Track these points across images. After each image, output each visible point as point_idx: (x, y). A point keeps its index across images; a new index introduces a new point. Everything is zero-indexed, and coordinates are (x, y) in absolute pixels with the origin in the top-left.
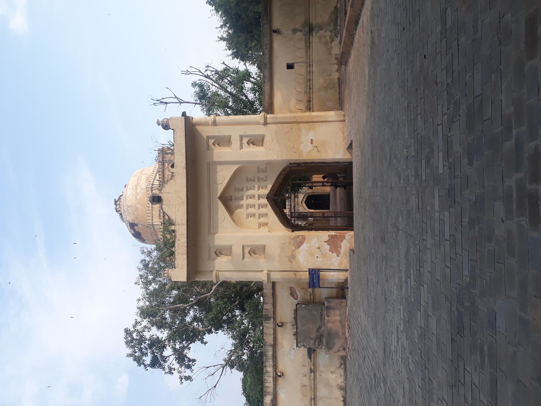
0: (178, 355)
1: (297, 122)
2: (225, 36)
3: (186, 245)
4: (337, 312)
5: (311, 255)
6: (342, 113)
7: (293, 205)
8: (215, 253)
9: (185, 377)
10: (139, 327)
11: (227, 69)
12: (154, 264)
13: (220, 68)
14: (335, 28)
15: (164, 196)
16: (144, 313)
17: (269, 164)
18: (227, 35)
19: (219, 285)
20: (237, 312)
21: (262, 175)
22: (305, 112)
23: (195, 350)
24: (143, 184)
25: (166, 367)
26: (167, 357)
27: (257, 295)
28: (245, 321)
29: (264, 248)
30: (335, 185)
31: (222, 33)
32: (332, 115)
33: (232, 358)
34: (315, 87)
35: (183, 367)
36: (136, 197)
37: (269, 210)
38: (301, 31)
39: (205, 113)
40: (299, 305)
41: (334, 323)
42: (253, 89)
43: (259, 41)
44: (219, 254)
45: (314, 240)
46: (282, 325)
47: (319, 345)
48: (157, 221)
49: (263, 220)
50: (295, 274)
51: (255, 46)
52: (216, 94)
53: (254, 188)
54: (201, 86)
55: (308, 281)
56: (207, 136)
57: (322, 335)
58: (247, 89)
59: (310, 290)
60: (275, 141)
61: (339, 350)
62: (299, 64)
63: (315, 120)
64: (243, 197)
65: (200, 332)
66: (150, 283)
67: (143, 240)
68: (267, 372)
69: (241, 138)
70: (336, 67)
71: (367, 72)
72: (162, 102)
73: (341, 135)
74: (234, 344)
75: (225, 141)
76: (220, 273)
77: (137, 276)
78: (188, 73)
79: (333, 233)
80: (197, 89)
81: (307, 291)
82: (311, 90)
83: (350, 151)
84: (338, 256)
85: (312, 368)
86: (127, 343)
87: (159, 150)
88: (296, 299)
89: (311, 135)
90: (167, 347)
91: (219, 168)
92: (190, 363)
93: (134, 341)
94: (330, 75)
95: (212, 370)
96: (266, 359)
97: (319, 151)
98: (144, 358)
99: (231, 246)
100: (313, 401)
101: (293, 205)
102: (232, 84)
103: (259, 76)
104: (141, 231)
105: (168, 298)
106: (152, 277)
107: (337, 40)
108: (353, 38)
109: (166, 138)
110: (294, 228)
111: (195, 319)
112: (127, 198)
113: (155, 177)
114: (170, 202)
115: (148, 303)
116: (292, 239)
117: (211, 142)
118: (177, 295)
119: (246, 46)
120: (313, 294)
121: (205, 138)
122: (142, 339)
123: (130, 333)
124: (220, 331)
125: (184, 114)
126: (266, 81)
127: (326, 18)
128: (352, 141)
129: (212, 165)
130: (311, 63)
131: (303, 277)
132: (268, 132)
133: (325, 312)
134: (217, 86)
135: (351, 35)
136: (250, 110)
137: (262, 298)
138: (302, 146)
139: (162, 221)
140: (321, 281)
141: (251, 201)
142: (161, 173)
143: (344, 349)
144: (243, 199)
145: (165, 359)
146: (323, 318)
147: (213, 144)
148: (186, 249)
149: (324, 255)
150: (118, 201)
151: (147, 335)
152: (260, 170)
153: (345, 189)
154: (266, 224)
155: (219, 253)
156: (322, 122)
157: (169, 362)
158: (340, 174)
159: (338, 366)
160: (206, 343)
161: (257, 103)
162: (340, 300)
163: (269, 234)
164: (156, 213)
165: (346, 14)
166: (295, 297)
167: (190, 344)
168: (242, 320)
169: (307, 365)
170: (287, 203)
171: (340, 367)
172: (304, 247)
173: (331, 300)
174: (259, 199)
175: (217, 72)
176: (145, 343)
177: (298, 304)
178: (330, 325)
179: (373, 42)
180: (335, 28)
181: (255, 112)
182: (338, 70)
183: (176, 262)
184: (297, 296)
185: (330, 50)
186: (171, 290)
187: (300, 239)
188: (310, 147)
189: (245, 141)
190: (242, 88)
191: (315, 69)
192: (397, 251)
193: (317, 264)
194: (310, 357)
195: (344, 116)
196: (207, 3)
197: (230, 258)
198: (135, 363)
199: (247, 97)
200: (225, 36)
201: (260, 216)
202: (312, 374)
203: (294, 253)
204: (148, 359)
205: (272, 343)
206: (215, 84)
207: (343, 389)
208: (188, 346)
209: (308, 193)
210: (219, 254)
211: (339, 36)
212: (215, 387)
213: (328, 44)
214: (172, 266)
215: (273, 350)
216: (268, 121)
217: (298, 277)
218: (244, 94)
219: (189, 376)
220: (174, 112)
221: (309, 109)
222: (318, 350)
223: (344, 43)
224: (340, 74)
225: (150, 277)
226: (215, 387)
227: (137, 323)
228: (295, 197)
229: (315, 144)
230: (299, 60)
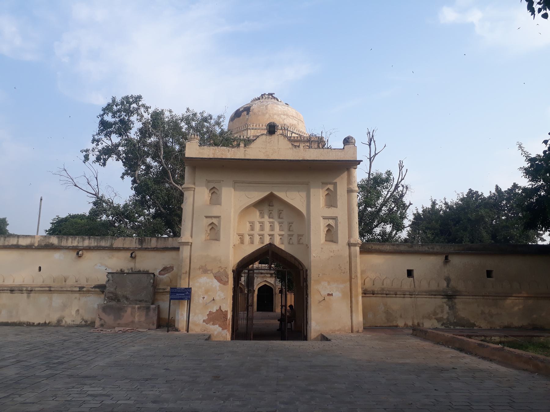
0: (112, 149)
2: (437, 207)
3: (224, 157)
4: (143, 319)
5: (207, 292)
6: (361, 329)
7: (263, 271)
8: (214, 187)
9: (88, 155)
10: (142, 110)
11: (405, 207)
12: (207, 127)
13: (406, 200)
14: (451, 324)
15: (275, 137)
16: (157, 116)
18: (438, 209)
19: (181, 192)
20: (152, 211)
21: (295, 239)
22: (362, 288)
23: (116, 166)
24: (288, 121)
26: (110, 137)
27: (170, 231)
28: (142, 218)
29: (217, 239)
30: (282, 319)
31: (439, 204)
32: (359, 318)
33: (104, 204)
34: (389, 301)
35: (98, 153)
36: (275, 114)
37: (257, 246)
38: (448, 286)
39: (360, 183)
40: (152, 276)
41: (132, 314)
42: (383, 233)
43: (432, 241)
44: (212, 191)
46: (133, 257)
47: (108, 298)
48: (251, 134)
49: (247, 239)
50: (186, 273)
51: (428, 238)
52: (379, 195)
54: (387, 180)
55: (178, 287)
56: (336, 183)
57: (119, 301)
58: (385, 227)
59: (168, 289)
60: (332, 254)
62: (412, 283)
63: (353, 299)
64: (272, 218)
65: (135, 171)
66: (188, 123)
67: (232, 119)
68: (84, 240)
69: (335, 218)
70: (410, 324)
71: (408, 361)
72: (371, 140)
74: (119, 206)
76: (192, 192)
77: (195, 111)
78: (401, 167)
79: (230, 316)
80: (384, 176)
81: (168, 286)
82: (385, 296)
83: (320, 338)
84: (204, 321)
85: (84, 289)
86: (127, 98)
87: (322, 138)
88: (160, 273)
89: (337, 294)
90: (120, 138)
91: (304, 194)
92: (102, 160)
93: (128, 106)
94: (401, 317)
95: (94, 183)
96: (98, 239)
97: (320, 302)
98: (110, 114)
99: (220, 204)
100: (47, 289)
101: (263, 271)
102: (389, 212)
103: (397, 241)
104: (241, 117)
105: (171, 140)
106: (194, 125)
107: (438, 325)
108: (443, 344)
109: (336, 143)
110: (237, 273)
111: (149, 167)
112: (275, 105)
113: (295, 133)
114: (269, 142)
115: (167, 120)
116: (225, 270)
117: (331, 187)
118: (174, 150)
119: (427, 228)
120: (164, 292)
121: (335, 181)
122: (129, 112)
123: (136, 101)
124: (133, 192)
125: (359, 162)
126: (395, 247)
127: (463, 314)
128: (330, 340)
129: (307, 187)
130: (413, 296)
131: (182, 281)
132: (341, 247)
133: (144, 305)
134: (388, 197)
135: (447, 343)
136: (363, 229)
137: (166, 236)
138: (326, 284)
140: (177, 301)
141: (267, 226)
143: (102, 325)
144: (269, 218)
145: (108, 135)
146: (138, 302)
147: (328, 189)
148: (220, 157)
149: (206, 305)
150: (273, 97)
151: (134, 118)
152: (300, 237)
153: (278, 330)
154: (242, 242)
155: (214, 191)
156: (351, 307)
157: (105, 139)
158: (294, 325)
159: (85, 318)
160: (122, 178)
161: (370, 236)
162: (155, 322)
163: (231, 246)
164: (258, 133)
165: (470, 337)
166: (163, 272)
167: (122, 160)
168: (144, 215)
169: (89, 283)
170: (264, 265)
171: (83, 320)
172: (216, 283)
173: (157, 312)
175: (402, 196)
176: (125, 115)
177: (154, 275)
178: (129, 310)
179: (442, 370)
180: (451, 324)
181: (361, 235)
182: (406, 326)
183: (206, 147)
185: (429, 318)
186: (179, 144)
188: (324, 293)
189: (332, 222)
190: (386, 222)
191: (408, 300)
192: (201, 396)
193: (197, 298)
194: (95, 287)
195: (358, 332)
196: (470, 189)
197: (208, 203)
198: (105, 105)
199: (376, 226)
200: (437, 207)
201: (251, 236)
202: (78, 289)
203: (209, 272)
204: (109, 118)
205: (114, 246)
206: (389, 195)
208: (120, 158)
209: (273, 291)
210: (212, 191)
211: (443, 327)
212: (75, 185)
213: (434, 315)
214: (203, 143)
215: (107, 247)
216: (352, 248)
217: (183, 276)
220: (361, 152)
221: (365, 293)
222: (103, 296)
223: (438, 334)
225: (194, 124)
226: (75, 185)
227: (147, 108)
228: (271, 274)
229: (327, 298)
230: (417, 283)
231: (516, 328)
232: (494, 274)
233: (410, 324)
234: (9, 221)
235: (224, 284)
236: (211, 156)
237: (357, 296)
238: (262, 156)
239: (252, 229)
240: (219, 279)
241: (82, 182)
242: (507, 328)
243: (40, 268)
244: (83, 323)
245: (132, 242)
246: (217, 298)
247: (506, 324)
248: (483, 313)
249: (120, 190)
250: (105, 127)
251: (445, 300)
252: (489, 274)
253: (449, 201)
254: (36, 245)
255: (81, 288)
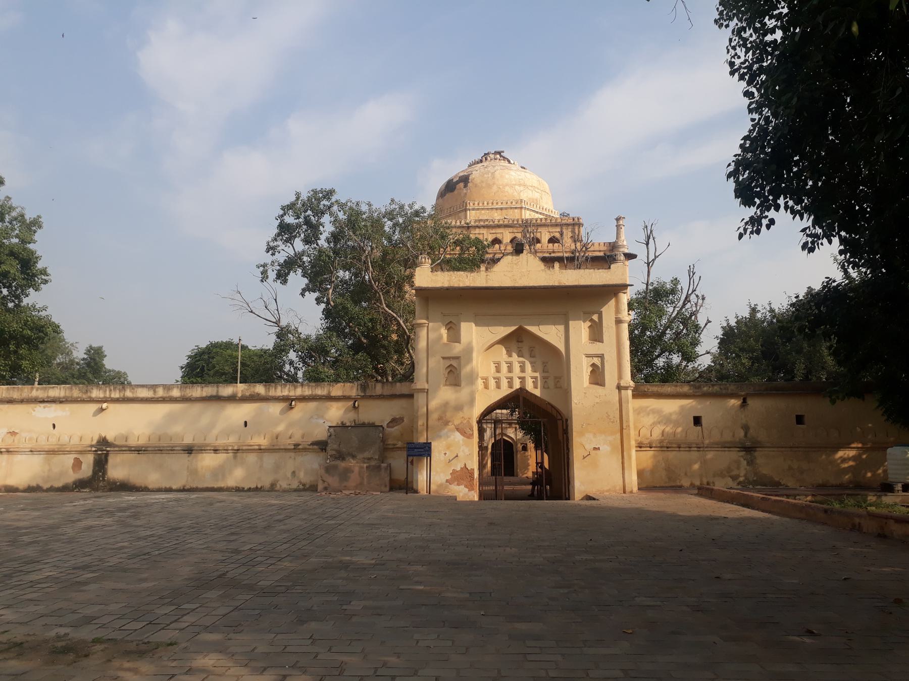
1: (622, 429)
2: (759, 315)
14: (750, 483)
17: (566, 393)
21: (551, 383)
22: (636, 441)
25: (276, 244)
36: (507, 185)
37: (505, 391)
38: (746, 435)
42: (668, 367)
45: (467, 451)
49: (492, 383)
52: (661, 313)
53: (534, 371)
54: (673, 291)
60: (598, 400)
61: (324, 481)
64: (522, 356)
69: (601, 357)
72: (649, 238)
73: (606, 488)
75: (596, 334)
78: (691, 273)
79: (476, 475)
80: (668, 286)
84: (447, 481)
86: (315, 192)
88: (388, 426)
89: (605, 448)
91: (561, 328)
95: (272, 306)
104: (456, 192)
107: (734, 485)
112: (506, 171)
116: (468, 422)
120: (395, 448)
122: (320, 213)
127: (765, 471)
132: (609, 391)
136: (639, 361)
139: (473, 223)
141: (517, 368)
142: (543, 221)
143: (326, 489)
156: (623, 463)
158: (554, 482)
160: (303, 295)
162: (388, 484)
166: (391, 425)
171: (300, 483)
174: (519, 378)
182: (692, 485)
184: (392, 427)
185: (721, 475)
187: (469, 431)
188: (589, 447)
190: (671, 351)
194: (313, 444)
196: (809, 288)
199: (659, 356)
200: (759, 315)
204: (290, 219)
205: (333, 394)
206: (676, 312)
207: (272, 488)
218: (662, 352)
219: (267, 277)
221: (640, 446)
222: (322, 454)
224: (688, 489)
229: (593, 453)
230: (706, 433)
231: (832, 486)
232: (806, 419)
233: (697, 483)
234: (106, 350)
235: (468, 438)
236: (446, 285)
237: (630, 449)
238: (507, 283)
239: (498, 370)
240: (463, 433)
241: (259, 308)
242: (823, 486)
243: (246, 423)
244: (301, 487)
245: (351, 389)
246: (461, 454)
247: (821, 482)
248: (790, 468)
249: (308, 316)
250: (286, 231)
251: (742, 453)
252: (800, 420)
253: (776, 307)
254: (240, 395)
255: (297, 445)
